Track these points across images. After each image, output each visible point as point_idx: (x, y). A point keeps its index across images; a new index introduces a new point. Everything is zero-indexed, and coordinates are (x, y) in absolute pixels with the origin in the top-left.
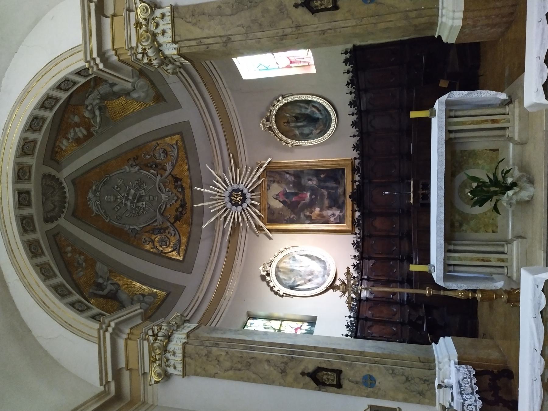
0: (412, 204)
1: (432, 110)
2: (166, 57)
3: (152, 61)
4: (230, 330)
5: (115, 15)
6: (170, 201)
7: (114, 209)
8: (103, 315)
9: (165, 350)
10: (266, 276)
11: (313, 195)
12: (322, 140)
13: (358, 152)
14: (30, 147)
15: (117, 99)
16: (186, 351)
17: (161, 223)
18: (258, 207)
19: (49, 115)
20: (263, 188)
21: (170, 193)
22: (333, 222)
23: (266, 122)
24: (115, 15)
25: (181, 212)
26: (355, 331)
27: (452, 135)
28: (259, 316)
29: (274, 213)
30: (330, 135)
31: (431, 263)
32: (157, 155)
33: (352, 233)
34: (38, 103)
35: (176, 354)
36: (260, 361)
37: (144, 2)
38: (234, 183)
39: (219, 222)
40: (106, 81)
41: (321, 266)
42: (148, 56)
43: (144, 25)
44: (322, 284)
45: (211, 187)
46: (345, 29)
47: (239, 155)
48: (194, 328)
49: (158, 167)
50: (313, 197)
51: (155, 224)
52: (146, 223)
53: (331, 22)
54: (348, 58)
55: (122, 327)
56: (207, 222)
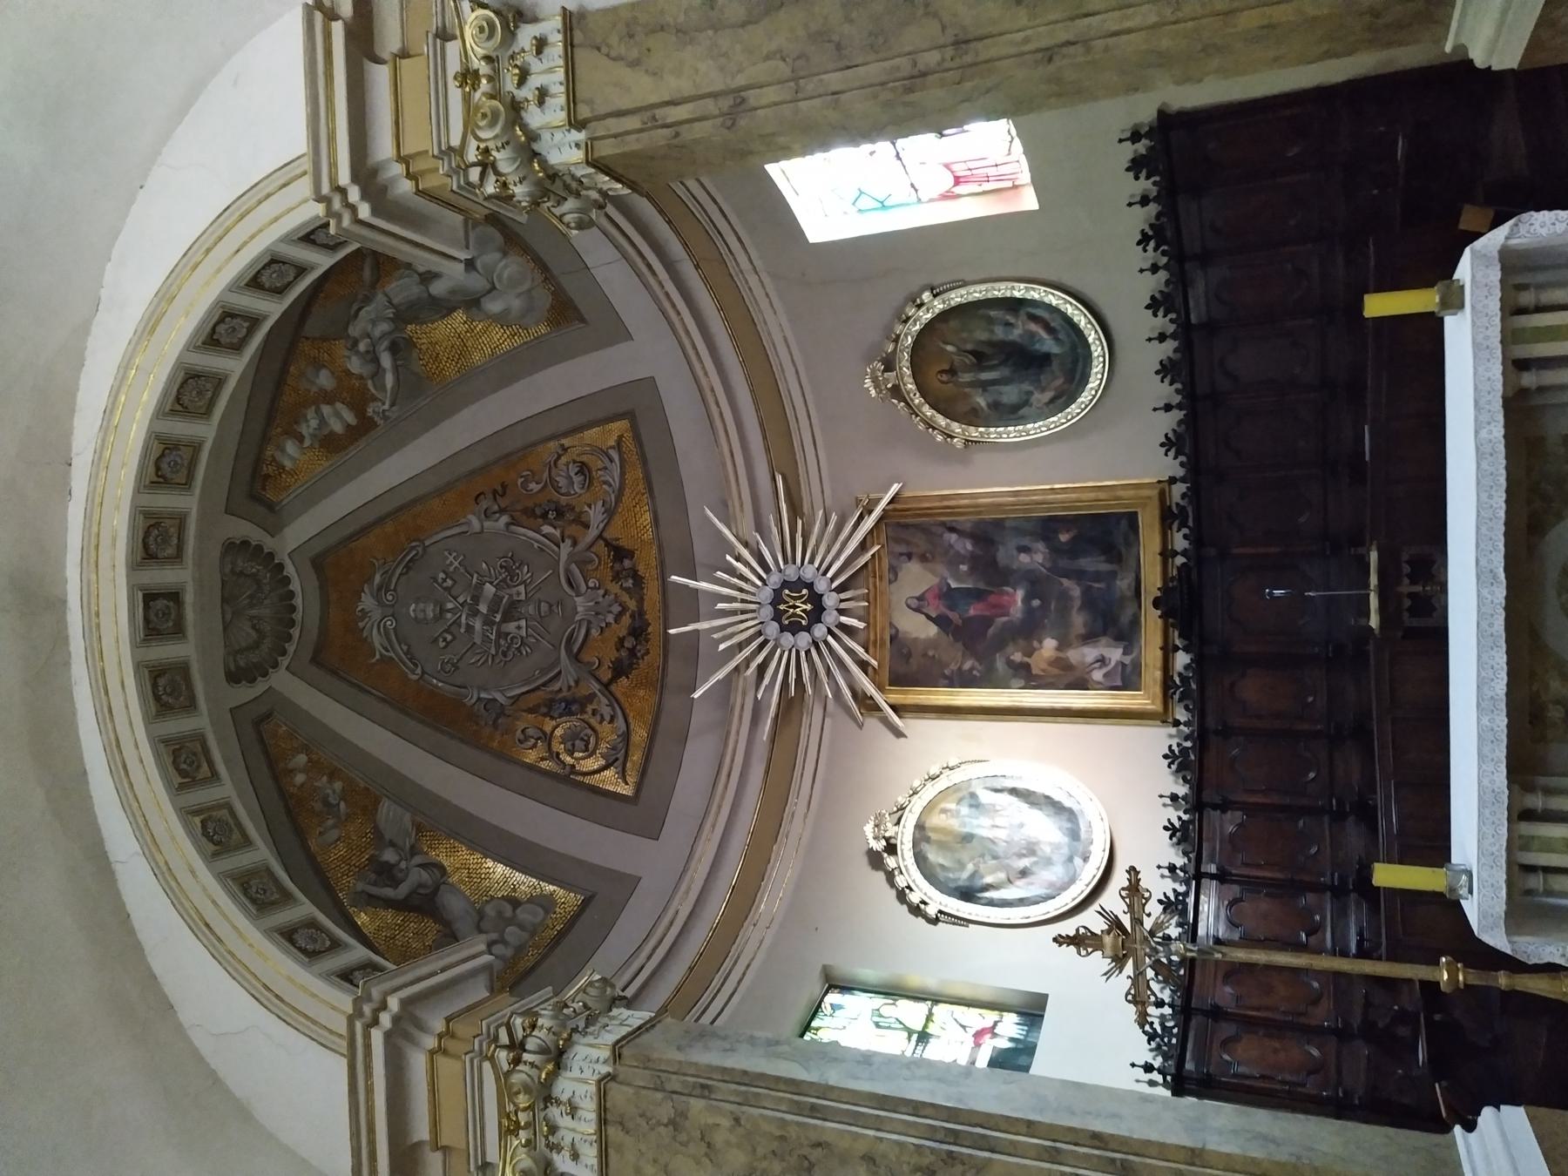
0: (1377, 632)
1: (1448, 287)
2: (553, 175)
3: (511, 187)
4: (752, 1041)
5: (404, 54)
6: (600, 616)
7: (435, 641)
8: (375, 968)
9: (545, 1095)
10: (885, 855)
11: (1034, 598)
12: (1063, 424)
13: (1182, 458)
14: (179, 461)
15: (443, 317)
16: (608, 1105)
17: (572, 684)
18: (862, 636)
19: (234, 367)
21: (601, 592)
22: (1099, 683)
23: (885, 370)
24: (404, 54)
26: (1175, 1053)
27: (1529, 379)
29: (909, 655)
31: (1455, 859)
32: (562, 482)
33: (1163, 722)
34: (197, 331)
35: (580, 1113)
36: (844, 1160)
37: (484, 6)
38: (786, 561)
40: (409, 266)
41: (1060, 829)
42: (497, 173)
43: (484, 76)
44: (1064, 887)
46: (1124, 38)
47: (801, 478)
48: (639, 1028)
50: (1036, 603)
51: (556, 686)
52: (530, 683)
53: (1072, 19)
55: (422, 1013)
56: (706, 680)
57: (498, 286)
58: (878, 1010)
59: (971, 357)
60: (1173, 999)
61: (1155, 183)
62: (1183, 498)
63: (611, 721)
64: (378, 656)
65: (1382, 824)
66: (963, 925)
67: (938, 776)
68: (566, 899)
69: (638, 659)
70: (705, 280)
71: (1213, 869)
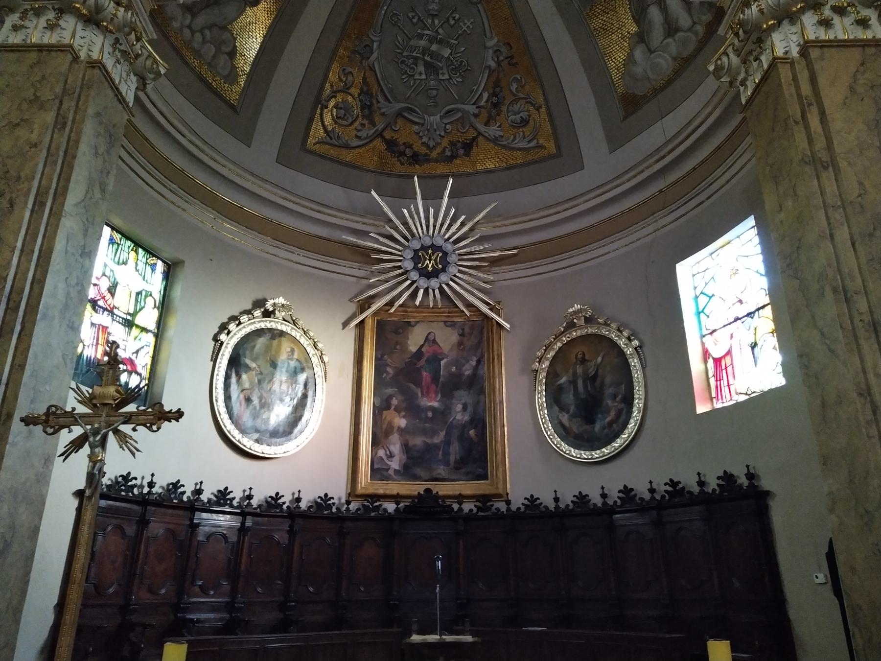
0: (408, 641)
3: (756, 4)
6: (426, 132)
7: (413, 10)
10: (263, 310)
11: (433, 414)
12: (547, 433)
13: (523, 509)
17: (382, 111)
18: (410, 303)
20: (449, 313)
22: (376, 454)
25: (403, 154)
28: (171, 286)
30: (558, 448)
32: (516, 107)
33: (349, 494)
35: (49, 33)
39: (382, 224)
47: (515, 266)
50: (430, 414)
54: (736, 481)
57: (652, 55)
58: (151, 295)
59: (593, 373)
60: (155, 494)
61: (714, 490)
62: (496, 509)
63: (357, 136)
65: (273, 637)
66: (212, 358)
67: (316, 348)
68: (234, 93)
69: (398, 157)
70: (653, 197)
71: (249, 523)
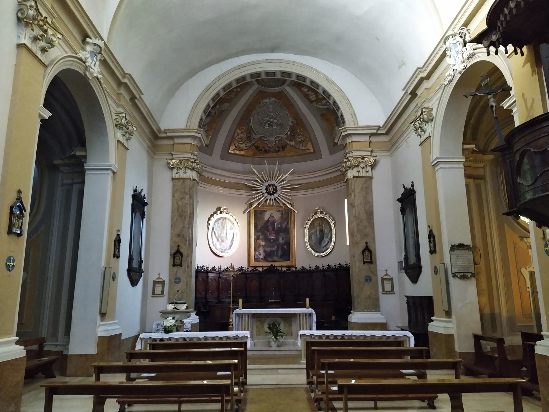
5: (370, 142)
7: (264, 111)
16: (186, 180)
17: (254, 138)
20: (278, 207)
21: (275, 144)
24: (370, 142)
25: (261, 150)
27: (298, 316)
29: (260, 214)
32: (300, 136)
35: (184, 174)
38: (281, 187)
39: (255, 177)
45: (279, 172)
49: (292, 137)
50: (272, 241)
51: (253, 134)
64: (261, 101)
